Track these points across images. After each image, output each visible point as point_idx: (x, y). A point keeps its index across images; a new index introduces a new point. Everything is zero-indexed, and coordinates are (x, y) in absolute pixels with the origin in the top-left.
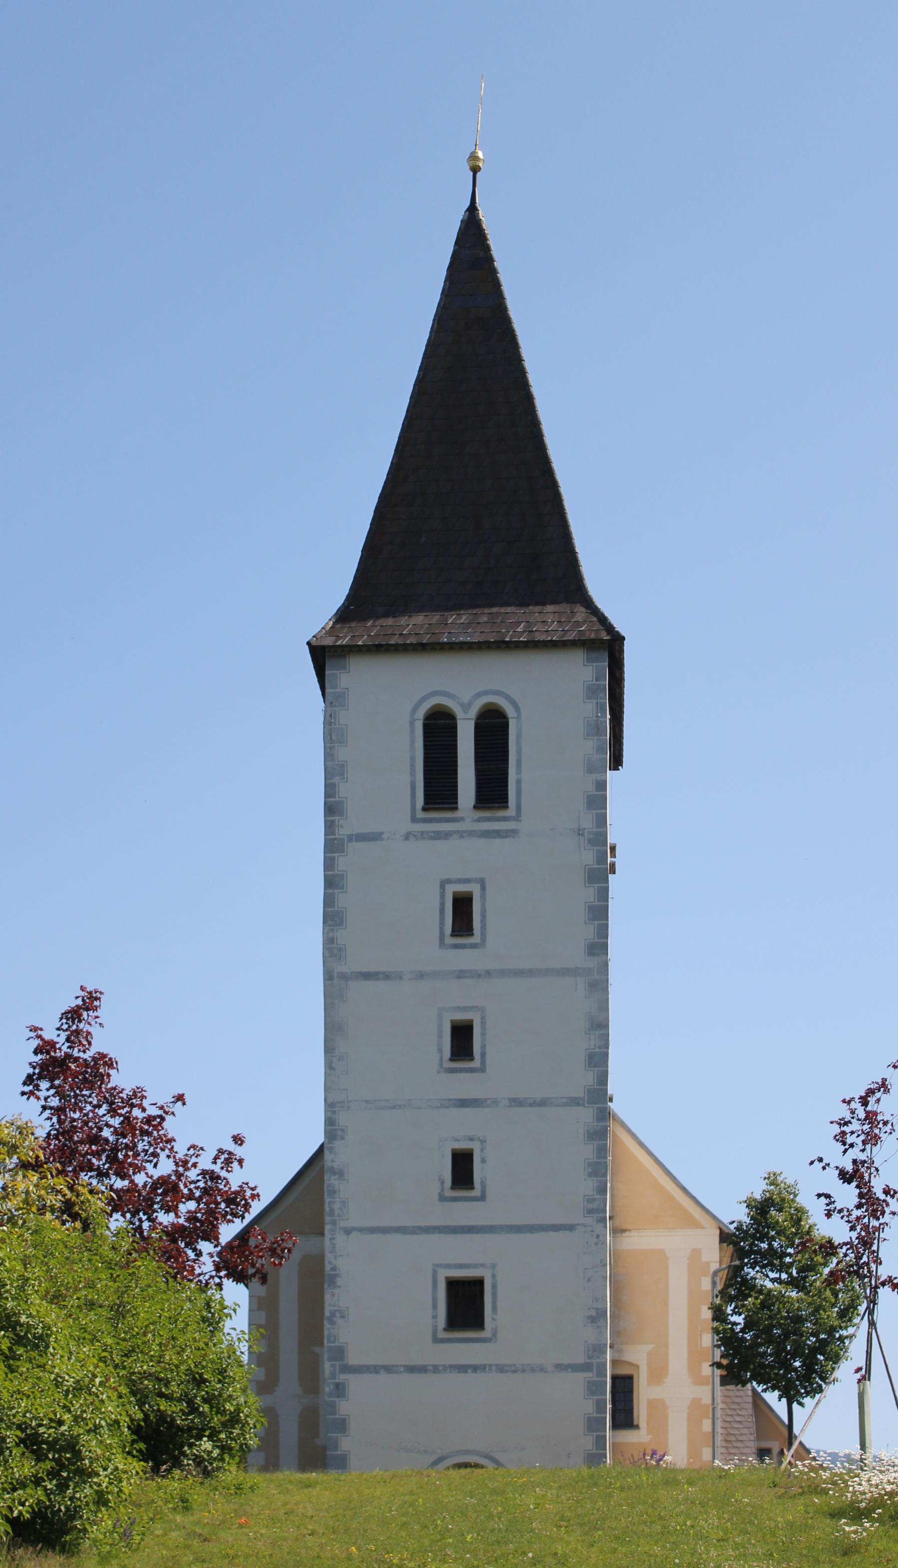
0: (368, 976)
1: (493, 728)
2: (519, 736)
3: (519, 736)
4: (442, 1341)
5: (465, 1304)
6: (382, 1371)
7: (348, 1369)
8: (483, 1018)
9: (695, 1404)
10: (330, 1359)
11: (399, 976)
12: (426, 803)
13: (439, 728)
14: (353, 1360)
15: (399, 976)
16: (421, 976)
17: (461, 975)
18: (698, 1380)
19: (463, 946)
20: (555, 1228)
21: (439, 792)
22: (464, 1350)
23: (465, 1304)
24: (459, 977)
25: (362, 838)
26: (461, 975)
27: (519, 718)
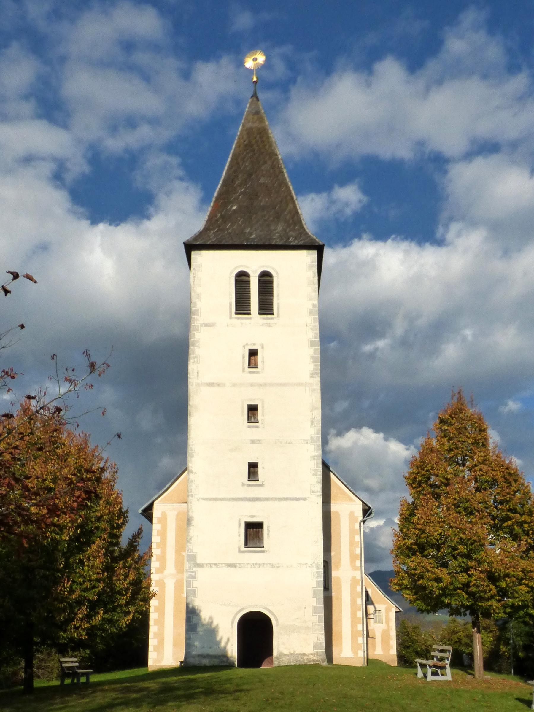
0: (211, 385)
1: (266, 280)
2: (278, 285)
3: (278, 285)
4: (244, 552)
5: (254, 531)
6: (214, 566)
7: (201, 566)
8: (263, 404)
9: (354, 579)
10: (188, 560)
11: (224, 385)
12: (236, 310)
13: (242, 279)
14: (199, 561)
15: (224, 385)
16: (234, 385)
17: (252, 385)
18: (355, 568)
19: (253, 372)
20: (296, 499)
21: (242, 306)
22: (252, 556)
23: (254, 531)
24: (252, 386)
25: (206, 325)
26: (252, 385)
27: (278, 277)
